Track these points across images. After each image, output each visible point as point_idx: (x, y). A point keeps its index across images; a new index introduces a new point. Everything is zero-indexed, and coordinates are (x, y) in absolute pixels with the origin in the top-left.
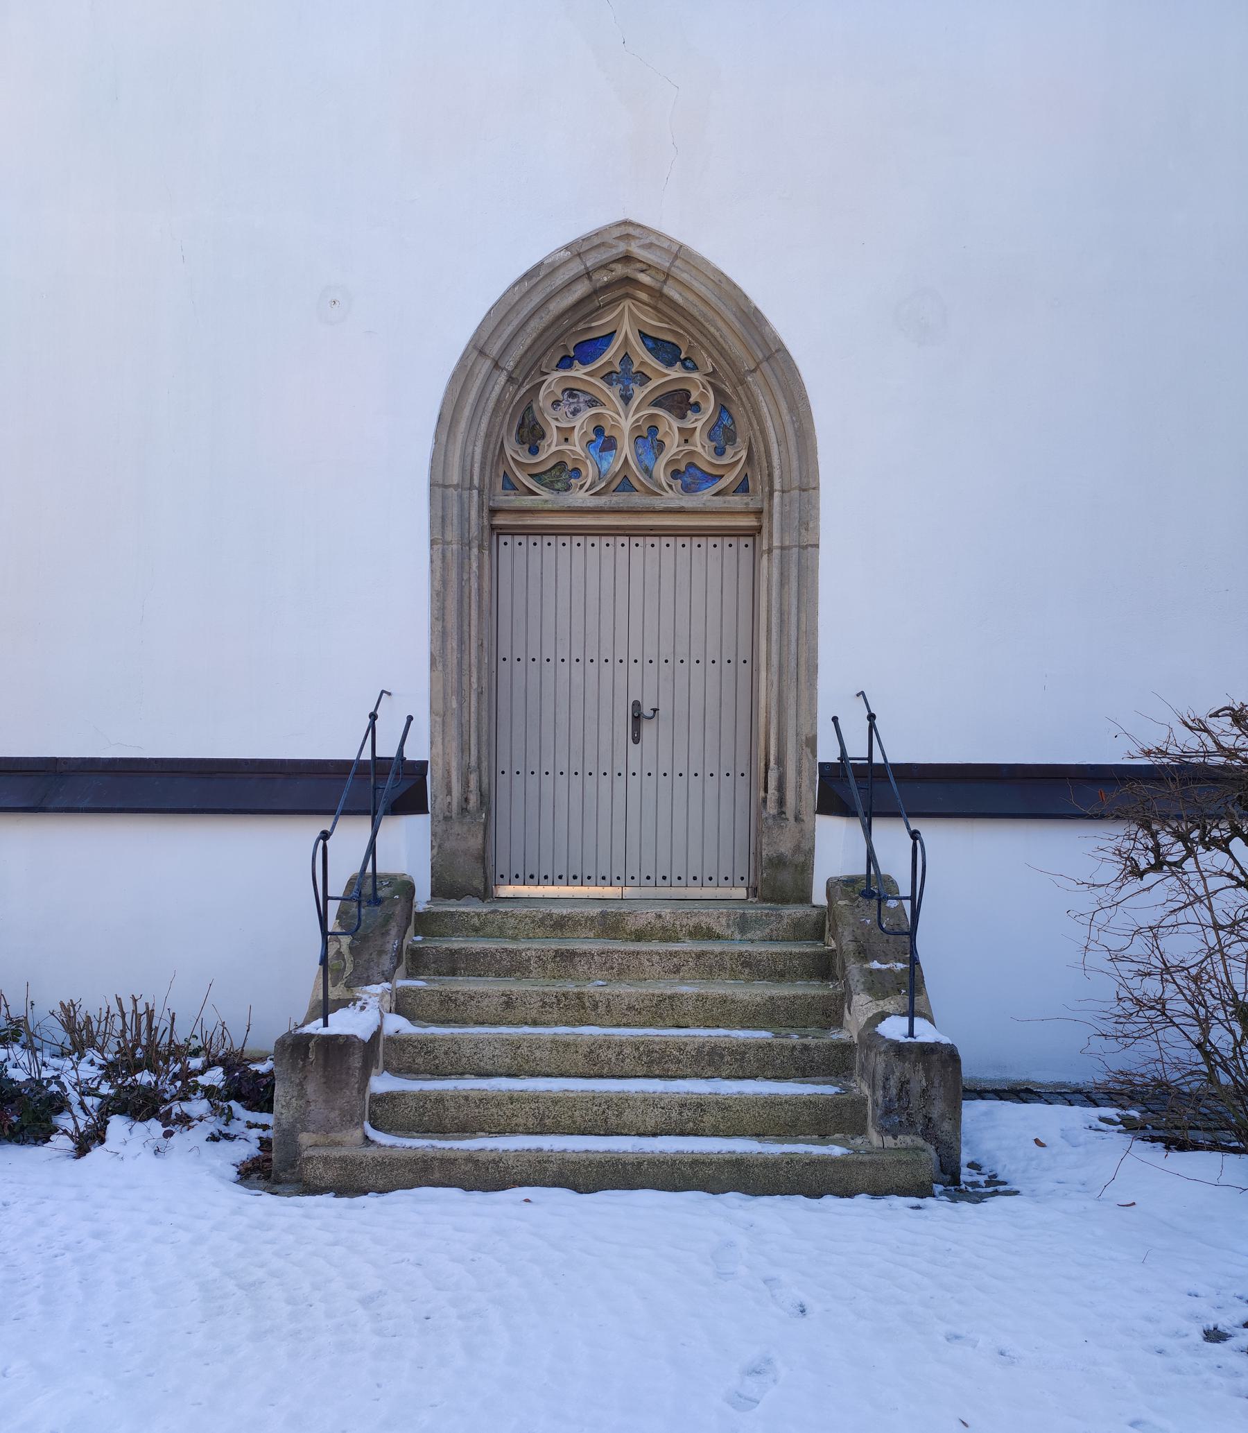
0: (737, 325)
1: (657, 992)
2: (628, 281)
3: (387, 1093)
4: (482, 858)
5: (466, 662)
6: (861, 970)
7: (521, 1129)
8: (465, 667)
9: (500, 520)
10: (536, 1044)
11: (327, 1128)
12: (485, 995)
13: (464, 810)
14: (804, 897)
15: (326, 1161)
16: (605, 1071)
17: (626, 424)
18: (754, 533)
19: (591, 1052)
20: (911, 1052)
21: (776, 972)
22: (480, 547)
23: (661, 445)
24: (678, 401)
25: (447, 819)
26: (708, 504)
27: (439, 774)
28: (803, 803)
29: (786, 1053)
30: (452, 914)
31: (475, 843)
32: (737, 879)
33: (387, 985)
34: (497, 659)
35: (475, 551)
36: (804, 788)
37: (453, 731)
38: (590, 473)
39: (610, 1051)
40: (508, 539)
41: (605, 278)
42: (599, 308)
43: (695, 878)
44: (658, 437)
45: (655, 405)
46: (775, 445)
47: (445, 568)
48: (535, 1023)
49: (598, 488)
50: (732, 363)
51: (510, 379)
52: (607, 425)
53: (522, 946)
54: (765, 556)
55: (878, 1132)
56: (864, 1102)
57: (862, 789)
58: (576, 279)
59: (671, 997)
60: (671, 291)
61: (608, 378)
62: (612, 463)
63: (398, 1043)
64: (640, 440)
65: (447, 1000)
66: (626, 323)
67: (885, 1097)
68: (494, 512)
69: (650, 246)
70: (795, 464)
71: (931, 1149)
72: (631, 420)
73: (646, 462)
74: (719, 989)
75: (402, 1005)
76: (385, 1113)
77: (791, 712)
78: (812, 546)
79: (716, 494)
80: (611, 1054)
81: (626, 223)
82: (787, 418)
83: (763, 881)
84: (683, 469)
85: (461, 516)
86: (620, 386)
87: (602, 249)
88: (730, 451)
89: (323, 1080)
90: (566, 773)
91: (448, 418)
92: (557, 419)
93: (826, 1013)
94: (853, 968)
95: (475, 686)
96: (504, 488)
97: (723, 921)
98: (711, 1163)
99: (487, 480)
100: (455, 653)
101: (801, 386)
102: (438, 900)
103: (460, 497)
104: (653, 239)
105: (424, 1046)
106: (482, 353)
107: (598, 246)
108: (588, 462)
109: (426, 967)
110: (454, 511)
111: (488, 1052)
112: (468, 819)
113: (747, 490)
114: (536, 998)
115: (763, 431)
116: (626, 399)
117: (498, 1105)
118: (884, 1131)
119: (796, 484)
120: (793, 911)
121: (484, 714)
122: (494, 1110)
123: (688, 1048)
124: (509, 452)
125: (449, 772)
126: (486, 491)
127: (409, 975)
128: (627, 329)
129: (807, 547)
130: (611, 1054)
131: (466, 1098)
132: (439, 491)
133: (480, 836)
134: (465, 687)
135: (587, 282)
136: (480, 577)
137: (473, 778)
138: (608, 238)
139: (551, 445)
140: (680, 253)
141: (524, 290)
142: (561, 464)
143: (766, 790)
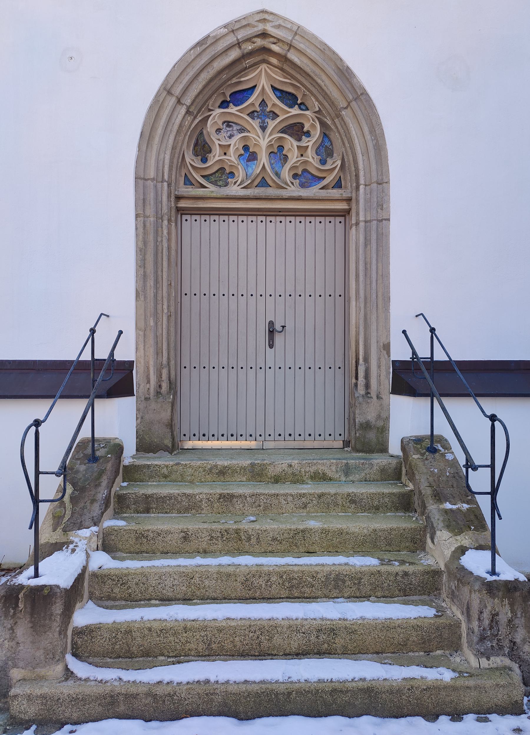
0: (335, 78)
1: (293, 527)
2: (265, 50)
3: (87, 627)
4: (170, 425)
5: (159, 295)
6: (439, 510)
7: (193, 653)
8: (159, 298)
9: (182, 204)
10: (205, 574)
11: (33, 664)
12: (168, 532)
13: (158, 393)
14: (383, 449)
15: (29, 698)
16: (257, 595)
17: (264, 143)
18: (345, 214)
19: (247, 580)
20: (498, 590)
21: (374, 507)
22: (169, 221)
23: (286, 158)
24: (296, 130)
25: (147, 399)
26: (317, 194)
27: (142, 369)
28: (382, 387)
29: (392, 578)
30: (149, 466)
31: (166, 415)
32: (337, 435)
33: (95, 529)
34: (181, 294)
35: (166, 222)
36: (383, 377)
37: (151, 341)
38: (240, 174)
39: (261, 580)
40: (188, 217)
41: (249, 47)
42: (246, 68)
43: (310, 435)
44: (284, 152)
45: (282, 132)
46: (361, 155)
47: (145, 233)
48: (205, 553)
49: (246, 184)
50: (332, 104)
51: (188, 112)
52: (251, 144)
53: (196, 491)
54: (354, 228)
55: (475, 655)
56: (458, 625)
57: (417, 377)
58: (230, 48)
59: (303, 531)
60: (293, 56)
61: (251, 114)
62: (256, 169)
63: (100, 577)
64: (272, 155)
65: (141, 536)
66: (263, 79)
67: (480, 627)
68: (178, 198)
69: (279, 26)
70: (374, 167)
71: (515, 667)
72: (267, 140)
73: (277, 169)
74: (338, 523)
75: (107, 545)
76: (86, 645)
77: (374, 327)
78: (385, 220)
79: (322, 188)
80: (262, 582)
81: (263, 12)
82: (368, 137)
83: (356, 439)
84: (300, 173)
85: (156, 199)
86: (259, 120)
87: (248, 28)
88: (330, 161)
89: (30, 625)
90: (226, 368)
91: (147, 134)
92: (219, 140)
93: (413, 541)
94: (432, 507)
95: (166, 311)
96: (185, 184)
97: (334, 468)
98: (347, 691)
99: (173, 177)
100: (152, 289)
101: (377, 117)
102: (141, 454)
103: (156, 186)
104: (281, 22)
105: (120, 579)
106: (169, 93)
107: (245, 26)
108: (239, 167)
109: (128, 507)
110: (151, 196)
111: (169, 583)
112: (161, 399)
113: (340, 187)
114: (206, 534)
115: (352, 148)
116: (263, 128)
117: (175, 634)
118: (480, 654)
119: (374, 179)
120: (379, 461)
121: (172, 329)
122: (172, 638)
123: (319, 576)
124: (188, 160)
125: (148, 368)
126: (173, 184)
127: (117, 515)
128: (264, 83)
129: (382, 220)
130: (262, 582)
131: (150, 629)
132: (141, 182)
133: (169, 410)
134: (159, 311)
135: (238, 50)
136: (169, 240)
137: (165, 372)
138: (252, 21)
139: (216, 156)
140: (298, 32)
141: (197, 53)
142: (222, 169)
143: (357, 378)
